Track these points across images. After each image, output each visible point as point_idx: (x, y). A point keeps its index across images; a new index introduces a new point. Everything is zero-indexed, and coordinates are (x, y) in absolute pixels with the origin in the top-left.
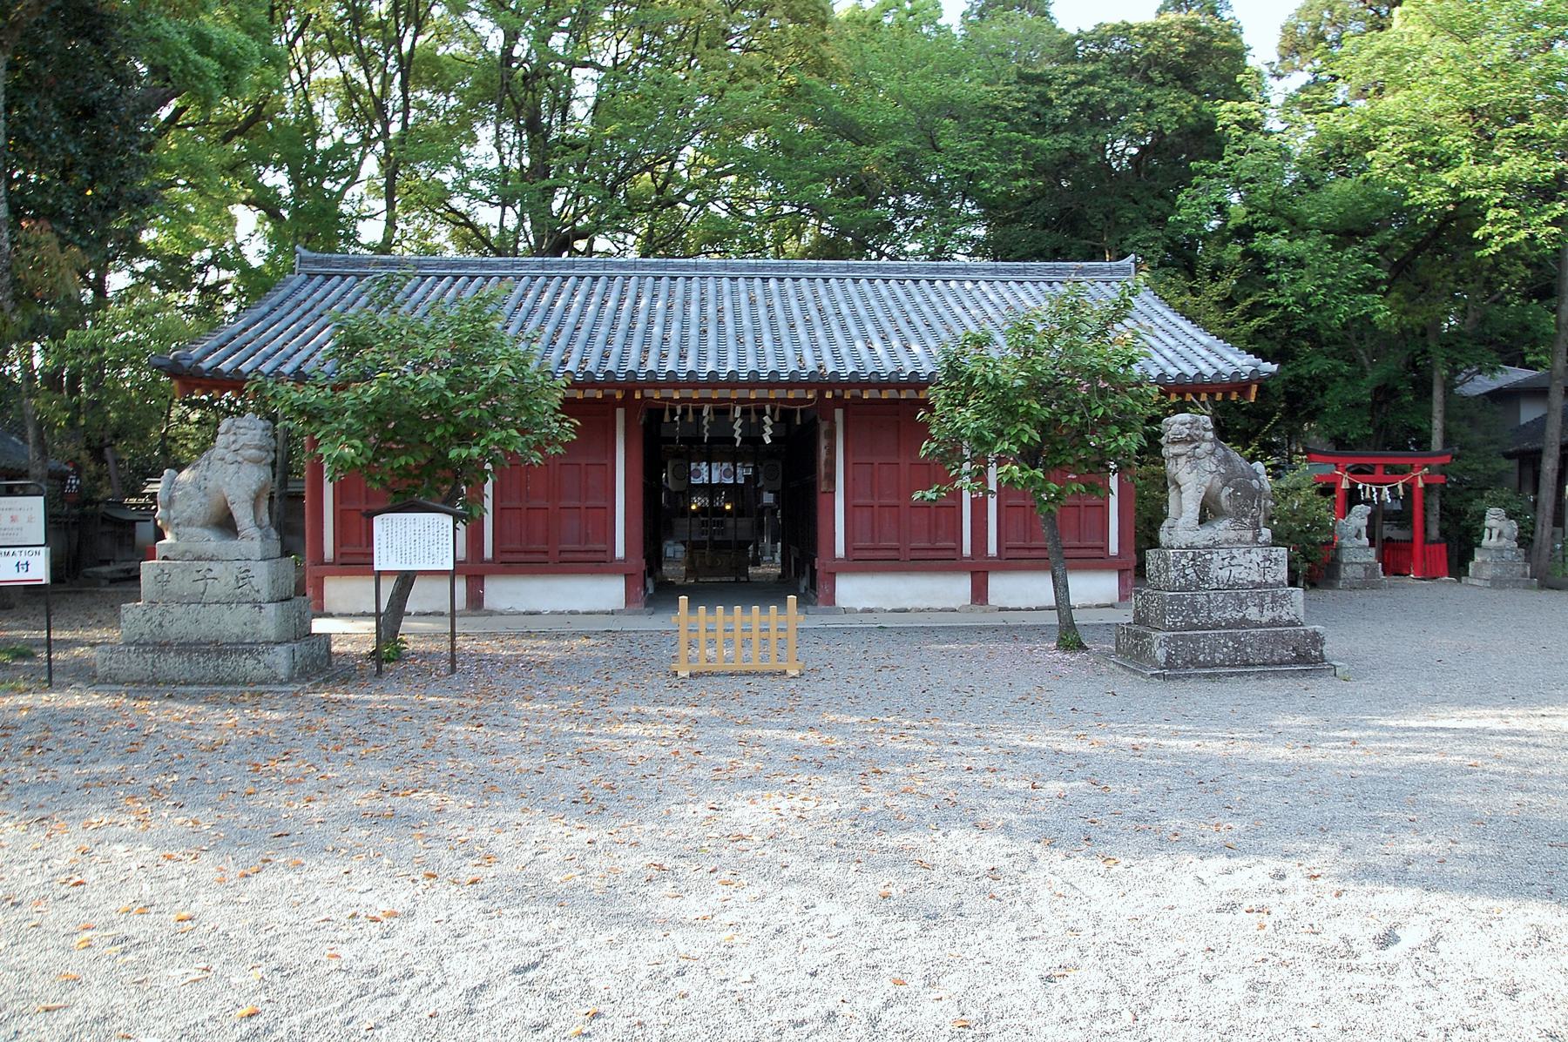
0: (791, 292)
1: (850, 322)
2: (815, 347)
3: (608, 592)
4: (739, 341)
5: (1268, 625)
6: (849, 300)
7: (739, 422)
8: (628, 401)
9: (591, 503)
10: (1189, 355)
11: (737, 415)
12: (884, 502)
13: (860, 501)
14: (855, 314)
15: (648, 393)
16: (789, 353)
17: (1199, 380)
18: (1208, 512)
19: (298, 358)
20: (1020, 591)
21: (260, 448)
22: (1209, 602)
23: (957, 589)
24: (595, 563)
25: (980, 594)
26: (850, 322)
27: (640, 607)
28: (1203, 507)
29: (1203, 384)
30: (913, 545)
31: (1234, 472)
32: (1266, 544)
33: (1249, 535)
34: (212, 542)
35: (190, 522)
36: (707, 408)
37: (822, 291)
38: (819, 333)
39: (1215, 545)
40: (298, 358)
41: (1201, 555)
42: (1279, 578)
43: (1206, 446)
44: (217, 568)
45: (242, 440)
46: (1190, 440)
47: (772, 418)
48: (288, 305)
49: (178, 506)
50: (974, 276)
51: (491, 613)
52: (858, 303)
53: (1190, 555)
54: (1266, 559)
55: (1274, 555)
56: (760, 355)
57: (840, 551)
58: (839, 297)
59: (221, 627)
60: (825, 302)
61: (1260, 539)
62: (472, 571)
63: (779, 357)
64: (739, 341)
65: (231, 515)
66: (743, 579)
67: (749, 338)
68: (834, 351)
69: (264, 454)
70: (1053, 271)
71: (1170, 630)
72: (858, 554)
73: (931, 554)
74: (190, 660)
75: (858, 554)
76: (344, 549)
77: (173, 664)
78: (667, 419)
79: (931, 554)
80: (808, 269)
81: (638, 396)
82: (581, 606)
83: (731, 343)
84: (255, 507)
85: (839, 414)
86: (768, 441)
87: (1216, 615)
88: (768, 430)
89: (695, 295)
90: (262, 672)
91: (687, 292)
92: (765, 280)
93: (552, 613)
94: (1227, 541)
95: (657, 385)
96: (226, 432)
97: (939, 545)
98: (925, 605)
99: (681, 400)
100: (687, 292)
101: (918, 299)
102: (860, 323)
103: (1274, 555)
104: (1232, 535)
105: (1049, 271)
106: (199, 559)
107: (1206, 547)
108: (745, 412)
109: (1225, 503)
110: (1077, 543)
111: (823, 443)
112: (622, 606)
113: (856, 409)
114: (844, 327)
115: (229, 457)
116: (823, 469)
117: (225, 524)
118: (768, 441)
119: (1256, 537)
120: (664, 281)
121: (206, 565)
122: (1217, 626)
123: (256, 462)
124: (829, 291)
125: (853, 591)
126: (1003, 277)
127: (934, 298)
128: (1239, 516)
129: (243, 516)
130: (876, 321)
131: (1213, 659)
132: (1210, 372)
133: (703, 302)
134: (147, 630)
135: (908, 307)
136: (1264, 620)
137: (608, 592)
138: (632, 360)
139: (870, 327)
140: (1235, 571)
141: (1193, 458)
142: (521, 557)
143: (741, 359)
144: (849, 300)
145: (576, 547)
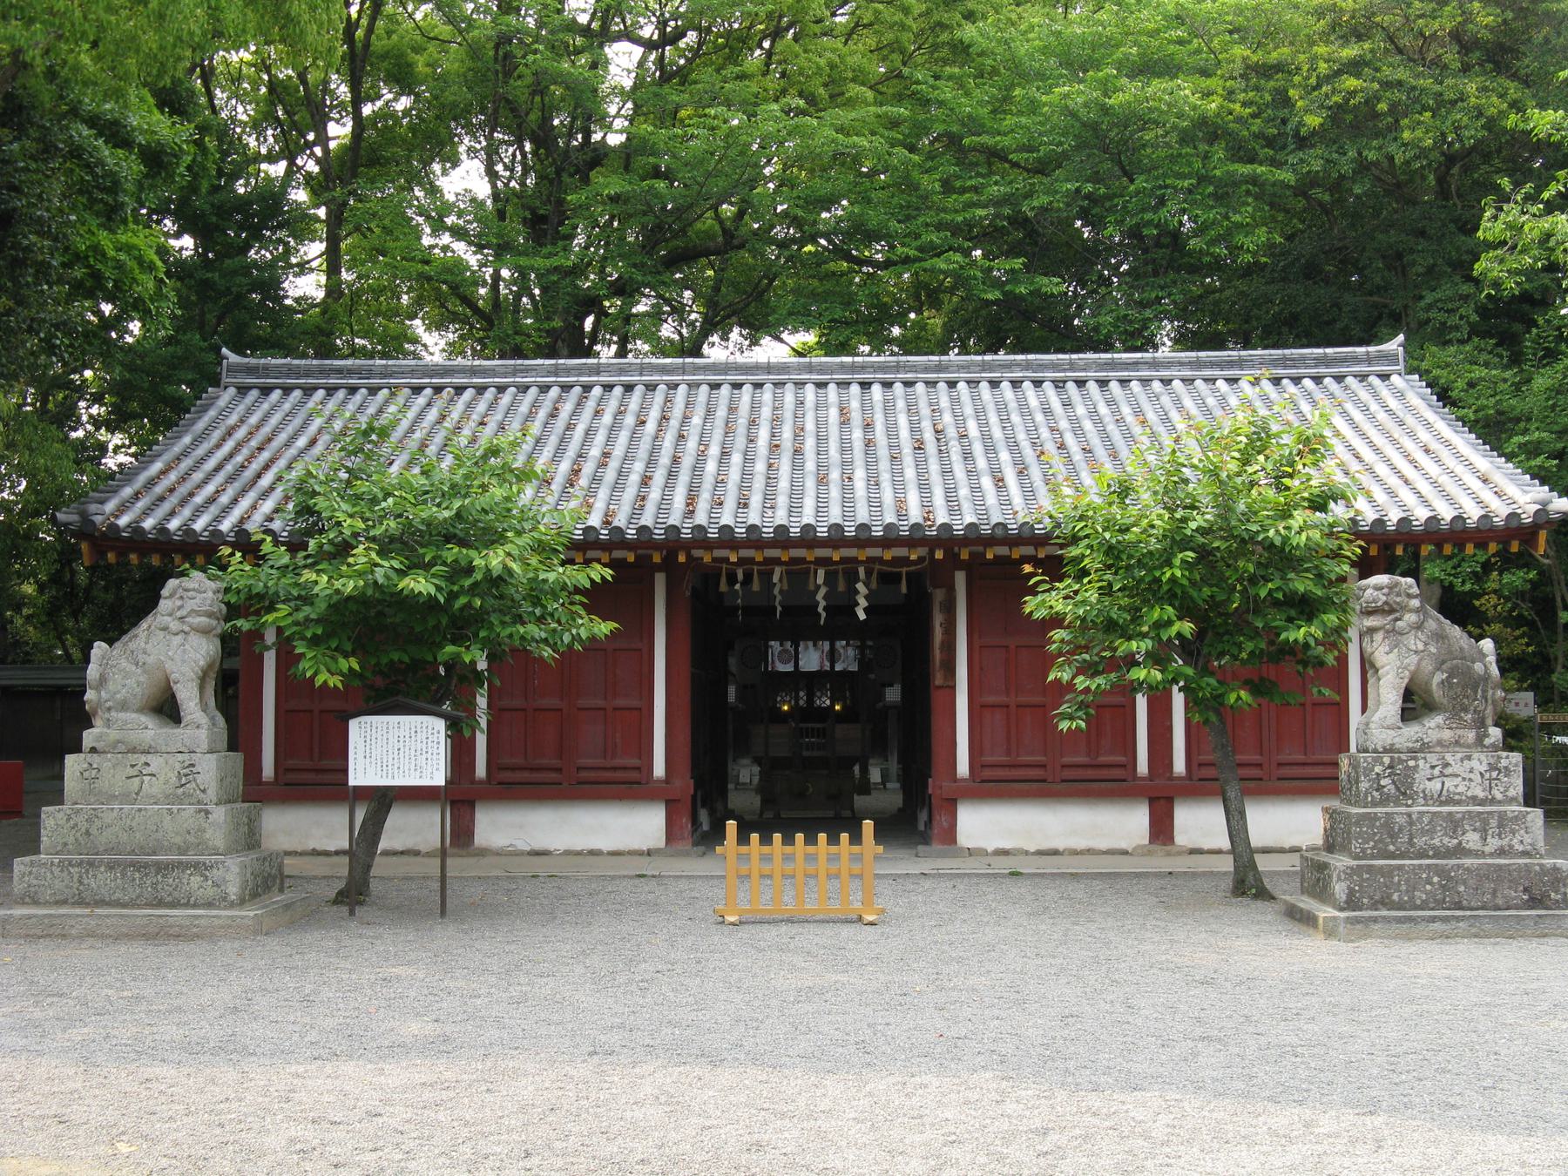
0: (901, 404)
1: (978, 449)
2: (924, 487)
3: (645, 825)
4: (822, 481)
5: (1491, 855)
6: (980, 413)
7: (823, 591)
8: (669, 564)
9: (621, 702)
10: (1452, 488)
11: (820, 580)
12: (1023, 699)
13: (991, 699)
14: (986, 437)
15: (697, 553)
16: (888, 495)
17: (1459, 526)
18: (1414, 704)
19: (237, 513)
20: (1200, 824)
21: (210, 615)
22: (1411, 823)
23: (1127, 824)
24: (625, 785)
25: (1162, 829)
26: (978, 449)
27: (686, 845)
28: (1408, 695)
29: (1465, 530)
30: (1067, 760)
31: (1450, 652)
32: (1494, 748)
33: (1471, 736)
34: (150, 729)
35: (124, 706)
36: (778, 571)
37: (944, 402)
38: (934, 467)
39: (1424, 747)
40: (237, 513)
41: (1401, 761)
42: (1512, 793)
43: (1411, 618)
44: (156, 762)
45: (191, 605)
46: (1387, 610)
47: (866, 585)
48: (217, 435)
49: (111, 686)
50: (1165, 373)
51: (484, 852)
52: (993, 419)
53: (1387, 760)
54: (1492, 767)
55: (1504, 763)
56: (847, 500)
57: (963, 767)
58: (968, 410)
59: (160, 835)
60: (947, 418)
61: (1487, 741)
62: (459, 798)
63: (875, 503)
64: (822, 481)
65: (173, 696)
66: (847, 813)
67: (835, 475)
68: (950, 494)
69: (214, 623)
70: (1283, 362)
71: (1357, 857)
72: (987, 773)
73: (1090, 773)
74: (123, 875)
75: (987, 773)
76: (291, 763)
77: (102, 881)
78: (723, 587)
79: (1090, 773)
80: (927, 369)
81: (682, 558)
82: (605, 844)
83: (810, 484)
84: (202, 688)
85: (960, 579)
86: (862, 616)
87: (1420, 842)
88: (863, 603)
89: (766, 412)
90: (210, 892)
91: (755, 407)
92: (866, 385)
93: (567, 853)
94: (1440, 743)
95: (707, 544)
96: (171, 596)
97: (1103, 759)
98: (1081, 844)
99: (742, 561)
100: (755, 407)
101: (1081, 410)
102: (990, 449)
103: (1504, 763)
104: (1447, 735)
105: (1275, 363)
106: (133, 751)
107: (1411, 751)
108: (830, 579)
109: (1437, 693)
110: (1300, 758)
111: (938, 619)
112: (661, 843)
113: (979, 570)
114: (967, 456)
115: (174, 625)
116: (937, 654)
117: (167, 708)
118: (862, 616)
119: (1480, 740)
120: (725, 390)
121: (143, 758)
122: (1422, 855)
123: (205, 632)
124: (955, 401)
125: (979, 825)
126: (1208, 373)
127: (1103, 409)
128: (1456, 710)
129: (189, 698)
130: (1014, 447)
131: (1412, 898)
132: (1394, 516)
133: (776, 421)
134: (71, 840)
135: (1064, 424)
136: (1487, 849)
137: (645, 825)
138: (667, 509)
139: (1004, 456)
140: (1449, 783)
141: (1392, 632)
142: (526, 776)
143: (821, 507)
144: (980, 413)
145: (599, 762)
